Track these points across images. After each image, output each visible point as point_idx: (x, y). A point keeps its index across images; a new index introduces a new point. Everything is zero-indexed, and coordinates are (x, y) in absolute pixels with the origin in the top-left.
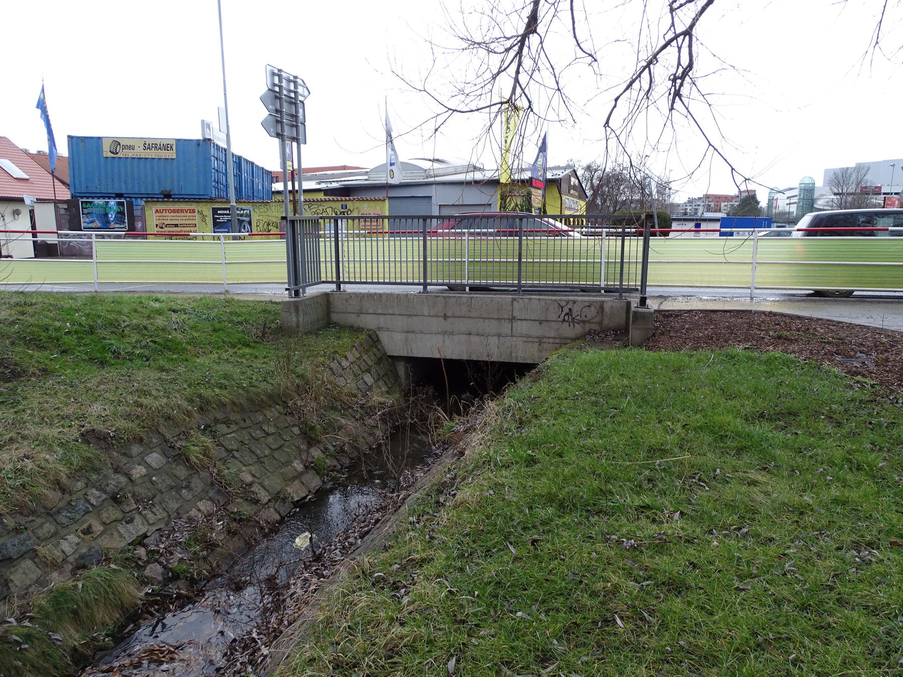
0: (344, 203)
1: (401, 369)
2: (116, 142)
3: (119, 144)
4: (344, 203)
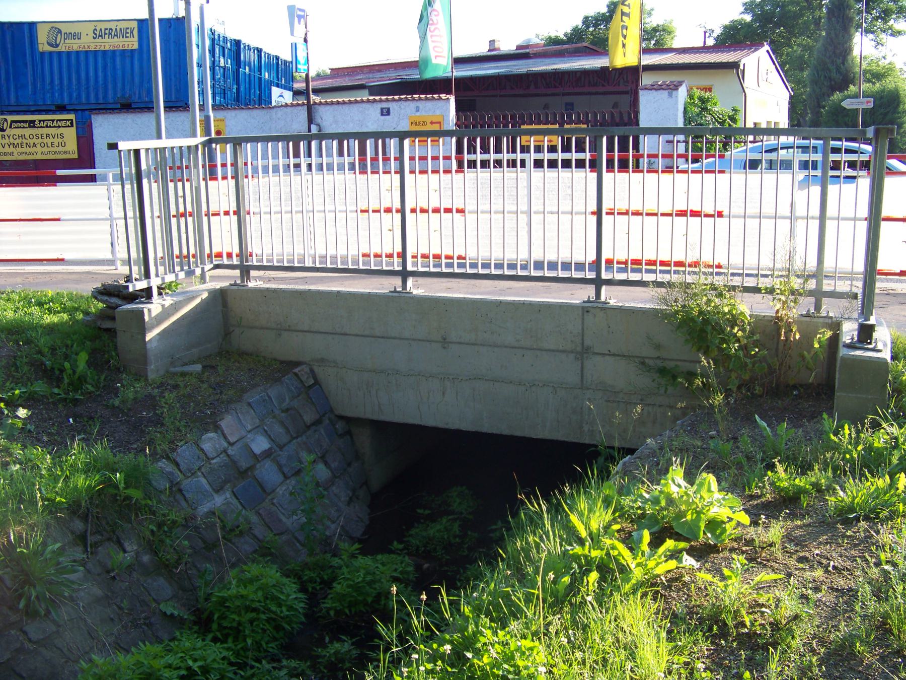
0: (385, 105)
1: (364, 440)
2: (55, 28)
3: (60, 31)
4: (385, 105)
